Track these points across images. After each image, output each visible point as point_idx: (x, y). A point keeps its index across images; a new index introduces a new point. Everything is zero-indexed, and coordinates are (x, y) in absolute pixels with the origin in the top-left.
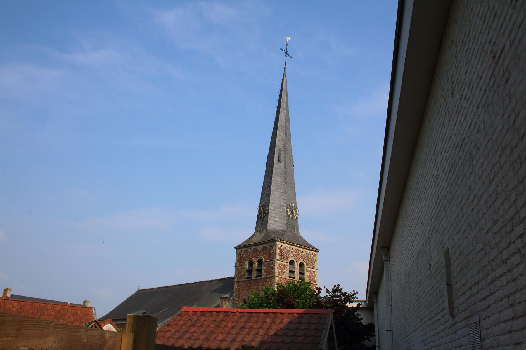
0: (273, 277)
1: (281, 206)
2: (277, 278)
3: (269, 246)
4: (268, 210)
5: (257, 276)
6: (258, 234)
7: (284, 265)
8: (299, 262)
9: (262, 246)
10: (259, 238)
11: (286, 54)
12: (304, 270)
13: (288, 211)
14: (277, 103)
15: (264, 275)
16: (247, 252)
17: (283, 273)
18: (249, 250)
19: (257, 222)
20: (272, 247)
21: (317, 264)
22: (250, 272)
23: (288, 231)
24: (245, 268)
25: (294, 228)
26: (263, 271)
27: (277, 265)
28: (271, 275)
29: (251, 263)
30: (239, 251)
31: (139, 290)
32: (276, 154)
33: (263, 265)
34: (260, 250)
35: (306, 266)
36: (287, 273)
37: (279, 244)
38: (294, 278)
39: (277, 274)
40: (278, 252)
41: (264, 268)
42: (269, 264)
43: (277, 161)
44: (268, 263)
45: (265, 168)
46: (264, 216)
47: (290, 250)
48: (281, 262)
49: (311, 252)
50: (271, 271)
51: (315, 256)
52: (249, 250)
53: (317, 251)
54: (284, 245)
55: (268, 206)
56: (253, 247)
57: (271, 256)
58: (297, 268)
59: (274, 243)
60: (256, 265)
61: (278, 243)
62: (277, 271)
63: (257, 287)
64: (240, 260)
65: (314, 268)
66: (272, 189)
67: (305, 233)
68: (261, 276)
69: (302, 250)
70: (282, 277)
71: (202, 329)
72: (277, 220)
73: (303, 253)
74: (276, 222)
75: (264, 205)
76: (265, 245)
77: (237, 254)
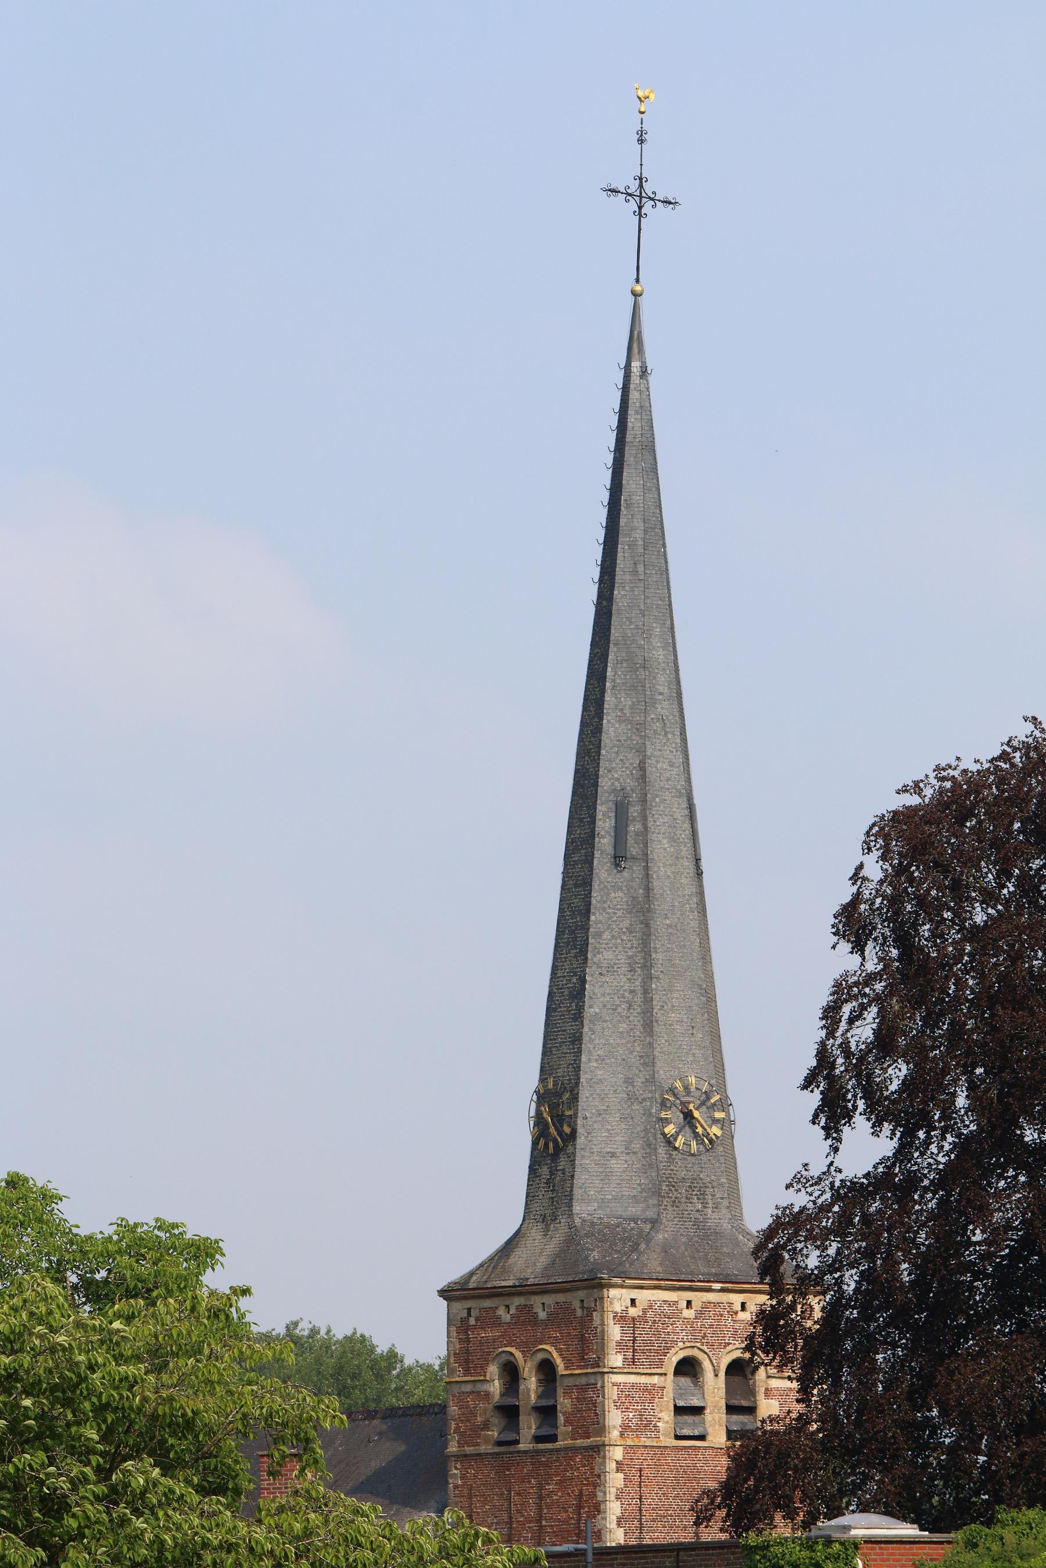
0: (598, 1450)
1: (631, 1098)
3: (577, 1304)
4: (572, 1121)
5: (538, 1439)
6: (535, 1234)
9: (549, 1300)
10: (533, 1262)
12: (752, 1393)
13: (666, 1121)
14: (604, 512)
16: (489, 1319)
17: (647, 1425)
18: (501, 1312)
19: (532, 1170)
20: (589, 1312)
24: (487, 1395)
26: (561, 1419)
27: (612, 1393)
29: (511, 1373)
30: (460, 1307)
32: (605, 824)
33: (560, 1391)
34: (542, 1315)
36: (666, 1418)
37: (617, 1298)
38: (702, 1438)
39: (615, 1434)
40: (615, 1332)
41: (564, 1403)
42: (583, 1389)
47: (676, 1315)
48: (632, 1379)
50: (590, 1420)
52: (501, 1312)
54: (644, 1296)
55: (575, 1098)
56: (518, 1301)
57: (587, 1347)
59: (596, 1293)
60: (531, 1384)
61: (613, 1292)
62: (614, 1418)
63: (541, 1487)
66: (591, 1010)
69: (737, 1299)
70: (644, 1441)
76: (561, 1298)
77: (450, 1322)
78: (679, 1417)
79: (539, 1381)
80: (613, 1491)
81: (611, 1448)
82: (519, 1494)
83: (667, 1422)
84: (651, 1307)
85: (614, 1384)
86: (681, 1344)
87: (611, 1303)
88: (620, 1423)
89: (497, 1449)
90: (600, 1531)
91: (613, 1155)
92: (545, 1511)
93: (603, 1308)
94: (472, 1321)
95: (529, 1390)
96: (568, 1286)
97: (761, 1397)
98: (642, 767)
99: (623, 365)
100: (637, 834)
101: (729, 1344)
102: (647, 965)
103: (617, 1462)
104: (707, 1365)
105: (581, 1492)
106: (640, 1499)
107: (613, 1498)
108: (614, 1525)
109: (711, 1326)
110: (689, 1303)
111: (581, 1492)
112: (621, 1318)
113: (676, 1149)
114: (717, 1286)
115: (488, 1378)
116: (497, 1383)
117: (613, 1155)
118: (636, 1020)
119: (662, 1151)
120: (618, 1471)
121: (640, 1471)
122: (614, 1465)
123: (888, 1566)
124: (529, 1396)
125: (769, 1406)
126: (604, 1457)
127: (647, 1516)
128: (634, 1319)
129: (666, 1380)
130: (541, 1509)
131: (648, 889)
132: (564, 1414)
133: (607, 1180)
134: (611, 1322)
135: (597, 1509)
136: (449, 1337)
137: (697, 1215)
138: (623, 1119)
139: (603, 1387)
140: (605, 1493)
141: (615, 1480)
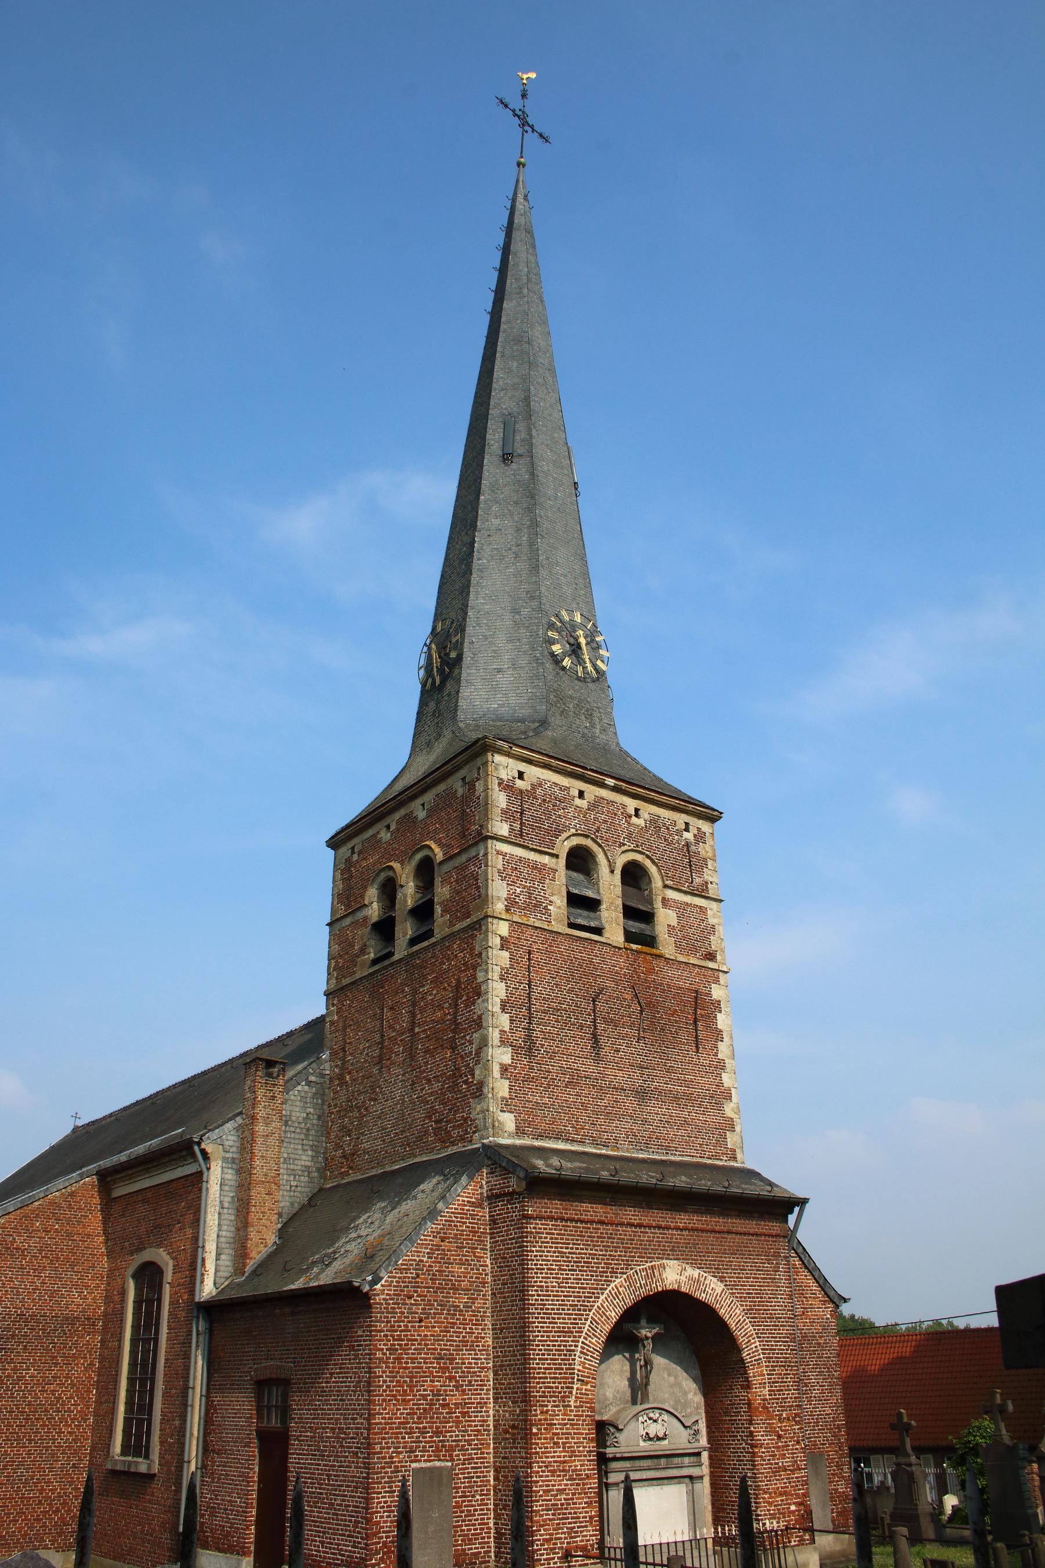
0: (480, 925)
4: (459, 646)
5: (413, 942)
7: (535, 866)
8: (621, 861)
9: (429, 797)
11: (524, 123)
13: (552, 642)
17: (537, 906)
18: (385, 836)
20: (471, 786)
22: (385, 929)
23: (556, 720)
24: (366, 919)
25: (589, 716)
26: (438, 909)
28: (474, 918)
31: (76, 1129)
32: (494, 437)
33: (438, 881)
34: (421, 814)
35: (657, 882)
36: (558, 904)
37: (503, 766)
38: (598, 931)
39: (500, 907)
40: (500, 800)
41: (442, 891)
43: (497, 460)
46: (443, 682)
48: (519, 852)
49: (681, 819)
53: (712, 816)
54: (534, 773)
58: (609, 887)
59: (479, 761)
60: (409, 893)
61: (498, 758)
62: (499, 890)
63: (415, 992)
65: (701, 892)
67: (642, 735)
68: (429, 934)
69: (631, 804)
72: (505, 680)
73: (640, 822)
76: (441, 788)
78: (572, 910)
79: (417, 887)
80: (497, 969)
81: (495, 921)
82: (392, 1009)
83: (559, 907)
84: (540, 785)
85: (498, 853)
86: (573, 831)
87: (496, 769)
88: (505, 896)
89: (377, 967)
90: (480, 1017)
91: (499, 671)
92: (419, 1017)
93: (487, 771)
94: (355, 857)
95: (405, 896)
96: (448, 767)
97: (658, 904)
98: (527, 400)
99: (511, 197)
100: (522, 440)
101: (624, 845)
102: (534, 524)
103: (502, 938)
104: (601, 858)
105: (458, 981)
106: (529, 985)
107: (496, 977)
108: (497, 1009)
109: (605, 822)
110: (581, 794)
111: (458, 981)
112: (507, 787)
113: (564, 668)
114: (610, 782)
115: (366, 902)
116: (375, 905)
117: (499, 671)
118: (523, 565)
119: (549, 665)
120: (502, 948)
121: (530, 953)
122: (497, 941)
123: (580, 1565)
124: (406, 901)
125: (667, 916)
126: (487, 931)
127: (534, 996)
128: (521, 791)
129: (557, 863)
130: (413, 1015)
131: (533, 474)
132: (441, 904)
133: (488, 692)
134: (496, 787)
135: (478, 992)
136: (334, 881)
137: (586, 731)
138: (510, 641)
139: (486, 854)
140: (487, 971)
141: (499, 958)
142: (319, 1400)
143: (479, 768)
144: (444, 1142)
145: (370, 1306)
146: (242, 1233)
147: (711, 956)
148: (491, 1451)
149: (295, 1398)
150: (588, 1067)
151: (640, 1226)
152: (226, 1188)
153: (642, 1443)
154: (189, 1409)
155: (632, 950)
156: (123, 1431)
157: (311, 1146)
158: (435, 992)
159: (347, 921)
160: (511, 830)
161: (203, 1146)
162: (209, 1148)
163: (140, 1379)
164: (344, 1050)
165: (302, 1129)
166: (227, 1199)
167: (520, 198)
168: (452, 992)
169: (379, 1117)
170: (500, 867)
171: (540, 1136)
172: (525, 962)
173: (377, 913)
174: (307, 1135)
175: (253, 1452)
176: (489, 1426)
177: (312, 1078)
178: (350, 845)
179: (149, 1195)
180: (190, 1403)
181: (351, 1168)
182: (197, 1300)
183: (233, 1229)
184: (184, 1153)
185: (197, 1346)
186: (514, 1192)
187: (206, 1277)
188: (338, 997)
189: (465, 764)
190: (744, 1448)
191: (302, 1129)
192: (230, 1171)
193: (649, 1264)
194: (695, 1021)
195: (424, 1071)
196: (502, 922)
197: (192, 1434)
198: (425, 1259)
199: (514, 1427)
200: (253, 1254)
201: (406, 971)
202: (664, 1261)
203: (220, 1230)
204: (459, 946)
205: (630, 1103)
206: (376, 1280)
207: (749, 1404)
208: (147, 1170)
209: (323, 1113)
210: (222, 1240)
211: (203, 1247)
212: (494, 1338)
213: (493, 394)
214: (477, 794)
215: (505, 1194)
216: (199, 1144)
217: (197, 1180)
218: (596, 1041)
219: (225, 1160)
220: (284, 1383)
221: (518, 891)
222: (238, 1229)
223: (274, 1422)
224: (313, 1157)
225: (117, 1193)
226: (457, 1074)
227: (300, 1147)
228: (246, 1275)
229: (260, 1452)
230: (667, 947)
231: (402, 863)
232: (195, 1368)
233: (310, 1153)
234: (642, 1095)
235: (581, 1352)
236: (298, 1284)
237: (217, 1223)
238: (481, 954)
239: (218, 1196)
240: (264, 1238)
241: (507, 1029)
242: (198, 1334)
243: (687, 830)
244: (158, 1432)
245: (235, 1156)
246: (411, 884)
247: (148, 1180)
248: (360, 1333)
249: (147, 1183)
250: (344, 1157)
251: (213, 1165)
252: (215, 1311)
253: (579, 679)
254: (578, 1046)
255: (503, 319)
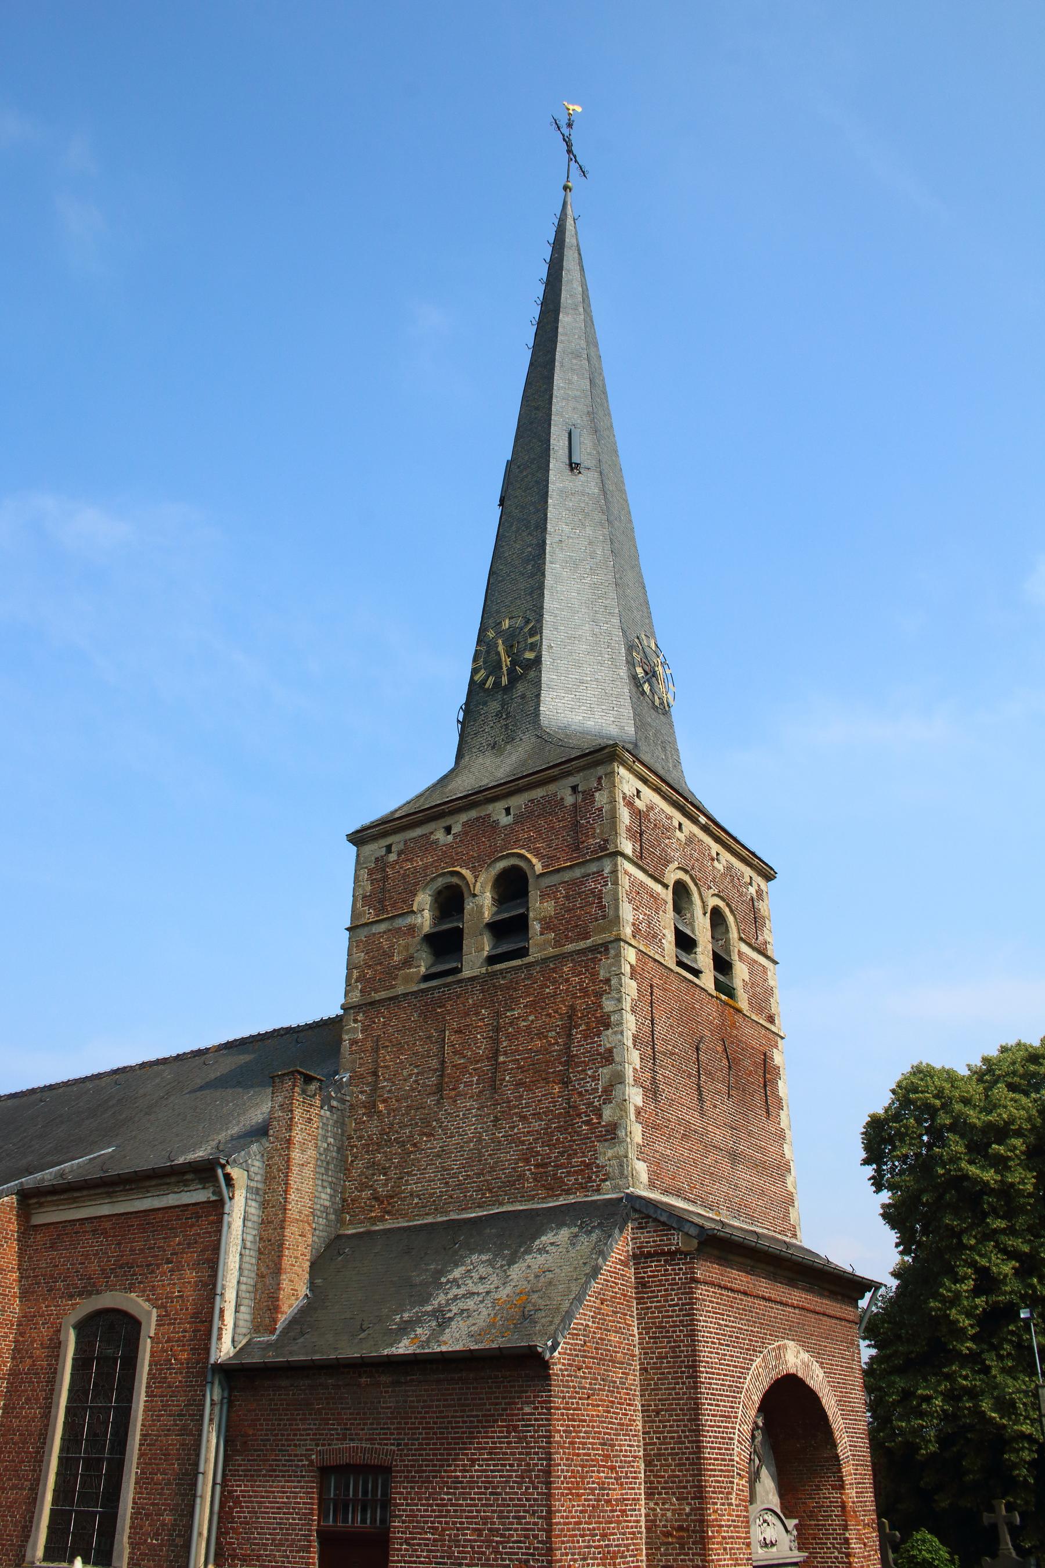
0: (610, 947)
2: (630, 955)
4: (536, 647)
5: (492, 960)
9: (518, 802)
15: (540, 942)
17: (654, 937)
18: (440, 836)
20: (589, 795)
21: (772, 935)
24: (412, 929)
25: (664, 749)
26: (535, 926)
29: (451, 901)
30: (376, 849)
33: (534, 894)
34: (505, 820)
40: (625, 816)
41: (540, 907)
44: (567, 876)
45: (495, 512)
46: (514, 679)
51: (759, 892)
53: (768, 875)
56: (464, 817)
58: (702, 929)
59: (600, 771)
60: (483, 903)
61: (622, 771)
62: (627, 912)
63: (498, 1015)
64: (379, 897)
68: (523, 952)
71: (753, 1200)
74: (578, 696)
75: (511, 638)
76: (538, 793)
81: (626, 946)
82: (459, 1031)
89: (423, 986)
90: (610, 1051)
95: (480, 908)
96: (555, 771)
105: (572, 1008)
108: (630, 1043)
111: (572, 1008)
114: (703, 820)
115: (415, 909)
116: (427, 914)
124: (482, 913)
130: (496, 1041)
142: (447, 1493)
143: (600, 778)
144: (552, 1189)
145: (548, 1377)
146: (268, 1280)
147: (771, 1019)
148: (644, 1558)
149: (400, 1493)
150: (694, 1119)
151: (769, 1300)
152: (249, 1224)
153: (760, 1551)
154: (198, 1500)
155: (721, 1000)
156: (49, 1527)
157: (330, 1183)
158: (531, 1018)
159: (382, 927)
160: (634, 851)
161: (229, 1169)
162: (235, 1172)
163: (83, 1458)
164: (375, 1074)
165: (322, 1161)
166: (249, 1238)
167: (570, 222)
168: (561, 1019)
169: (439, 1156)
170: (627, 888)
171: (665, 1192)
172: (649, 995)
173: (428, 923)
174: (327, 1169)
175: (313, 1558)
176: (641, 1527)
177: (334, 1103)
178: (389, 840)
179: (108, 1225)
180: (199, 1493)
181: (388, 1213)
182: (212, 1361)
183: (253, 1275)
184: (188, 1177)
185: (211, 1420)
186: (678, 1251)
187: (224, 1332)
188: (364, 1013)
189: (578, 772)
190: (836, 1558)
191: (322, 1161)
192: (254, 1204)
193: (776, 1344)
194: (765, 1086)
195: (515, 1107)
196: (630, 948)
197: (200, 1534)
198: (590, 1324)
199: (680, 1528)
200: (285, 1308)
201: (482, 991)
202: (786, 1341)
203: (241, 1275)
204: (573, 969)
205: (726, 1165)
206: (554, 1348)
207: (843, 1507)
208: (109, 1195)
209: (342, 1145)
210: (243, 1287)
211: (222, 1294)
212: (645, 1422)
213: (554, 400)
214: (597, 805)
215: (663, 1253)
216: (223, 1167)
217: (216, 1209)
218: (700, 1094)
219: (249, 1188)
220: (382, 1471)
221: (641, 917)
222: (260, 1276)
223: (355, 1521)
224: (331, 1196)
225: (38, 1219)
226: (571, 1112)
227: (320, 1182)
228: (278, 1332)
229: (320, 1559)
230: (743, 1003)
231: (473, 869)
232: (208, 1448)
233: (329, 1190)
234: (734, 1157)
235: (739, 1441)
236: (404, 1347)
237: (238, 1267)
238: (608, 981)
239: (240, 1233)
240: (295, 1289)
241: (638, 1067)
242: (212, 1404)
243: (751, 884)
244: (127, 1531)
245: (260, 1186)
246: (488, 895)
247: (106, 1207)
248: (527, 1410)
249: (105, 1210)
250: (376, 1199)
251: (237, 1193)
252: (237, 1376)
253: (655, 708)
254: (689, 1098)
255: (560, 330)
